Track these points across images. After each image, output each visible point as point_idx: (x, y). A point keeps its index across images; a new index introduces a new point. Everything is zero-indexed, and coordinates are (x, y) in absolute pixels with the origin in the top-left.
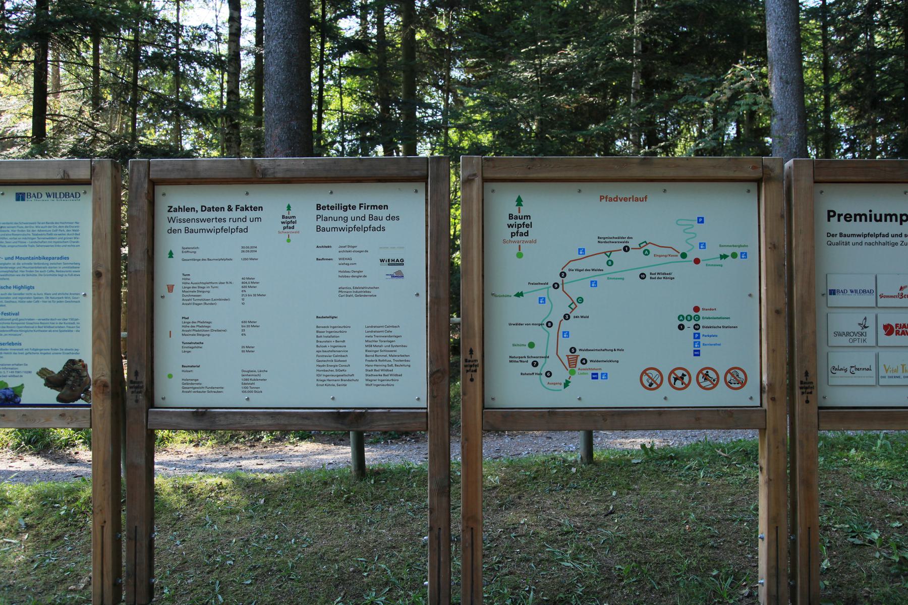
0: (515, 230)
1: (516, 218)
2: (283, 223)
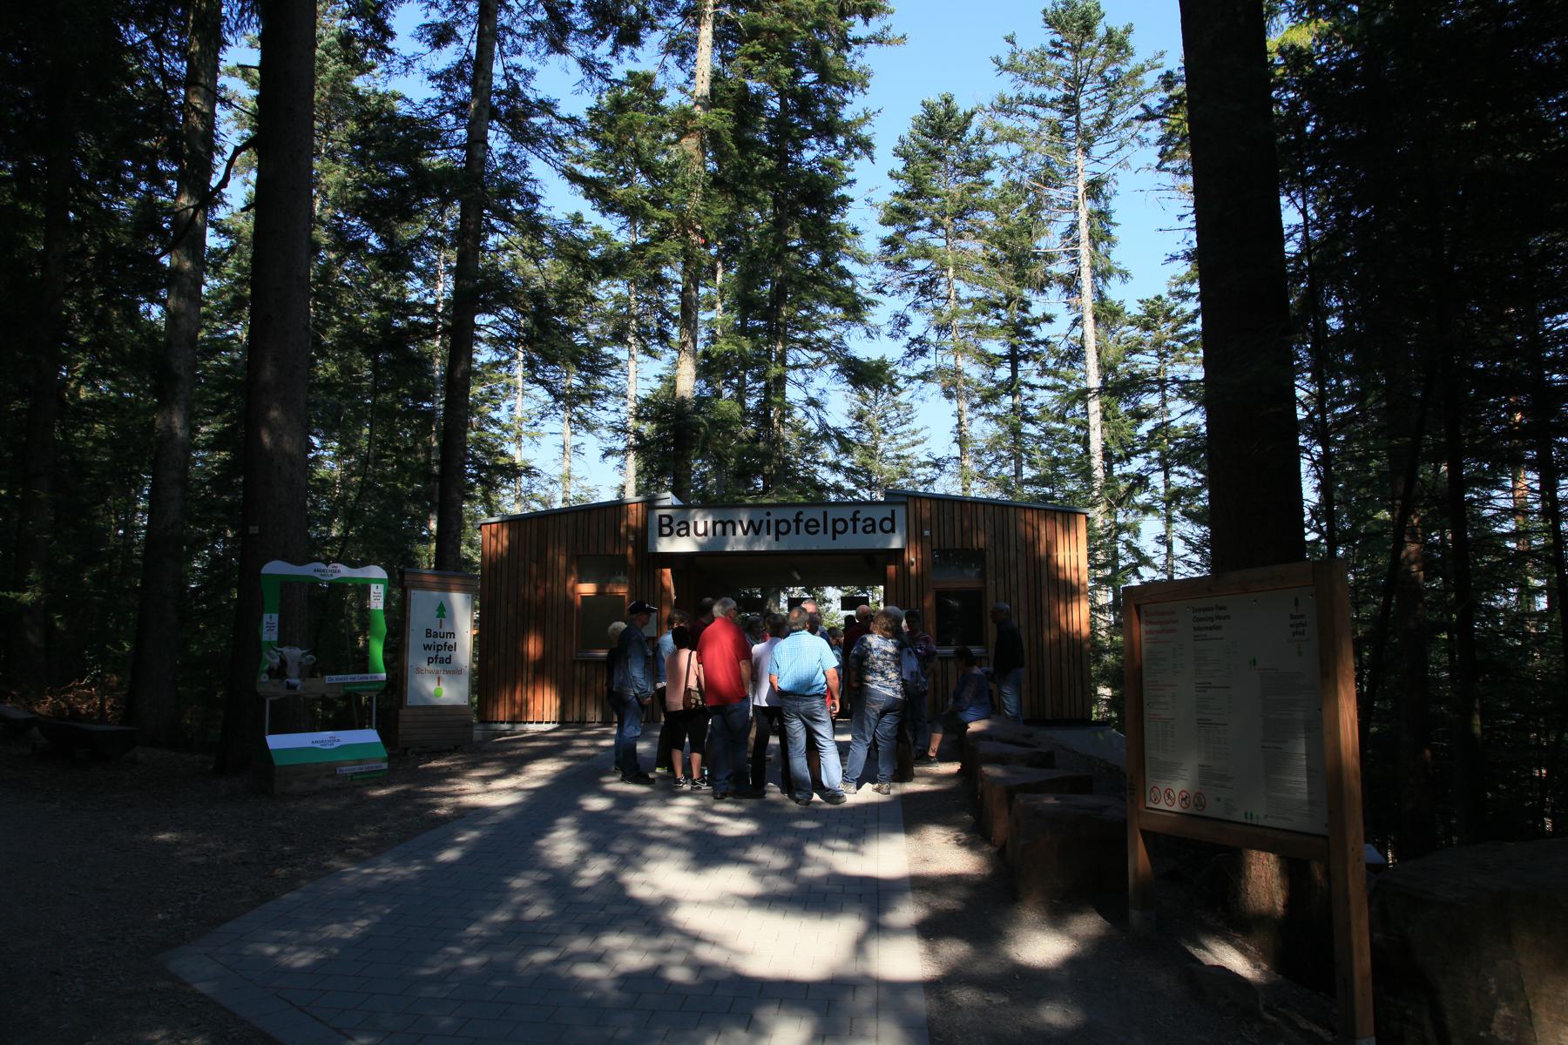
1: (436, 635)
2: (427, 647)
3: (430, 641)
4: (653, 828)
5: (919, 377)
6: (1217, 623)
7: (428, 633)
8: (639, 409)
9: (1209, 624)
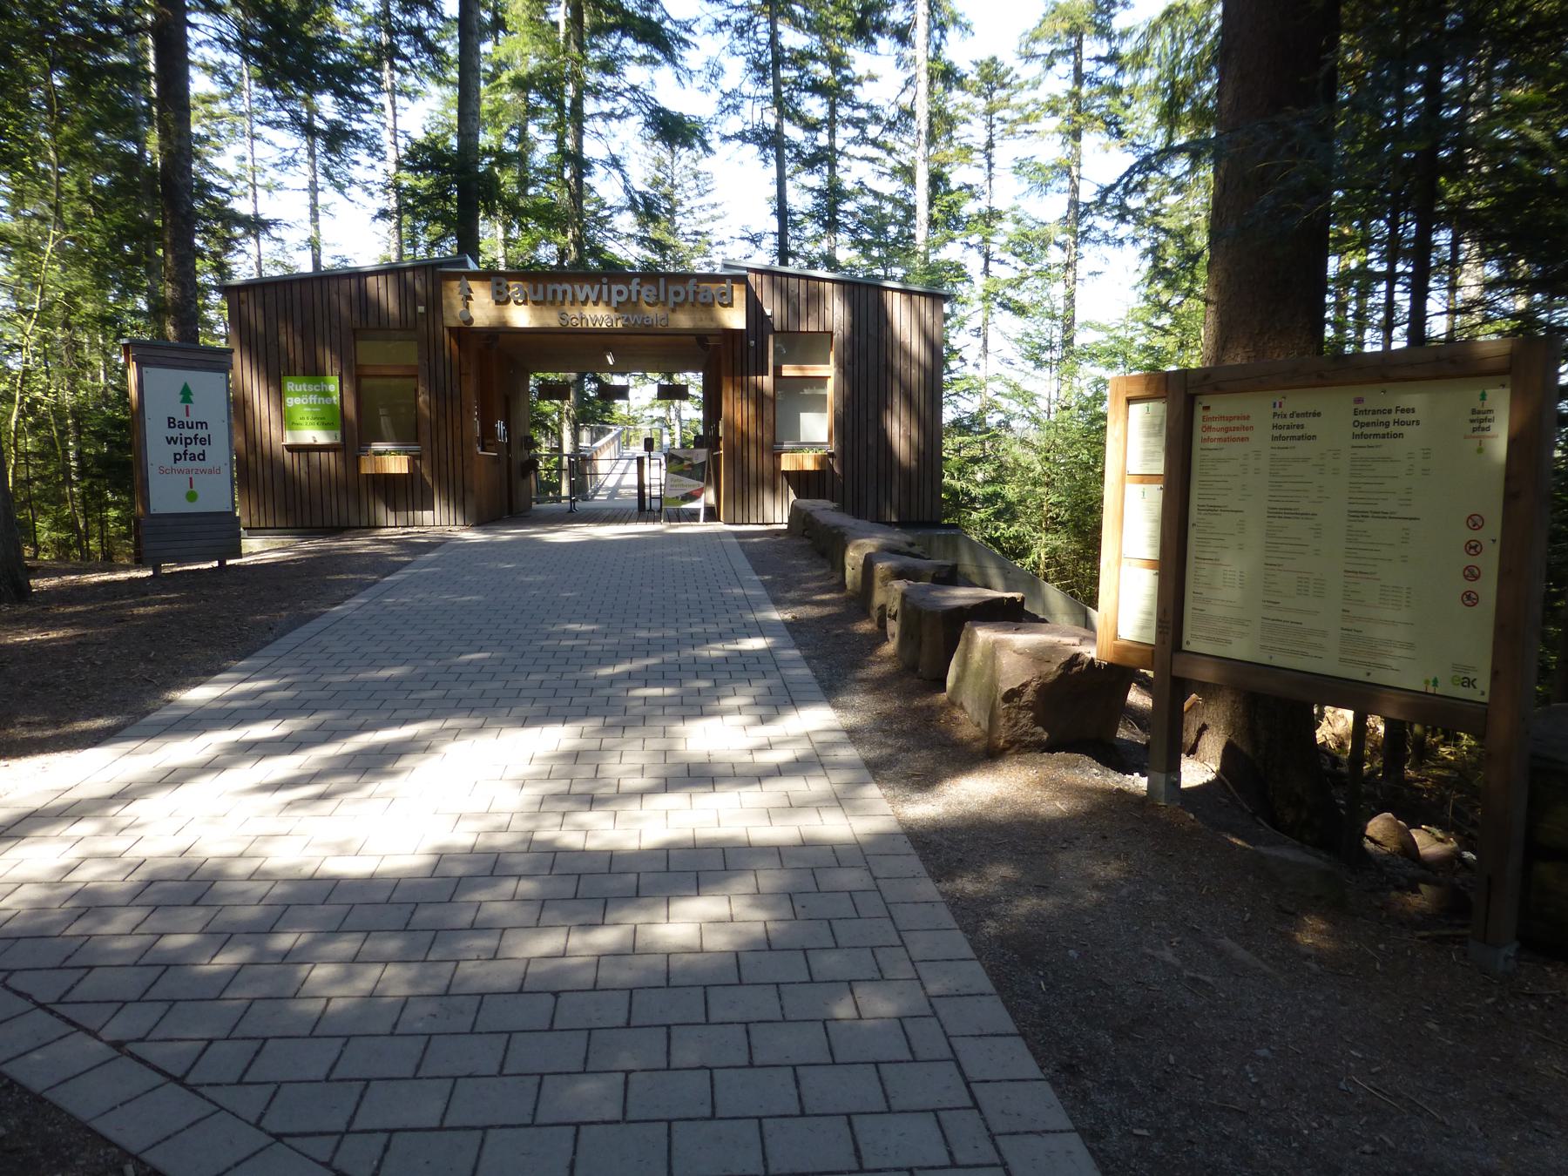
0: (180, 448)
1: (182, 425)
2: (170, 441)
3: (175, 433)
4: (739, 710)
5: (736, 136)
6: (1393, 429)
7: (171, 422)
8: (412, 156)
9: (1382, 430)
